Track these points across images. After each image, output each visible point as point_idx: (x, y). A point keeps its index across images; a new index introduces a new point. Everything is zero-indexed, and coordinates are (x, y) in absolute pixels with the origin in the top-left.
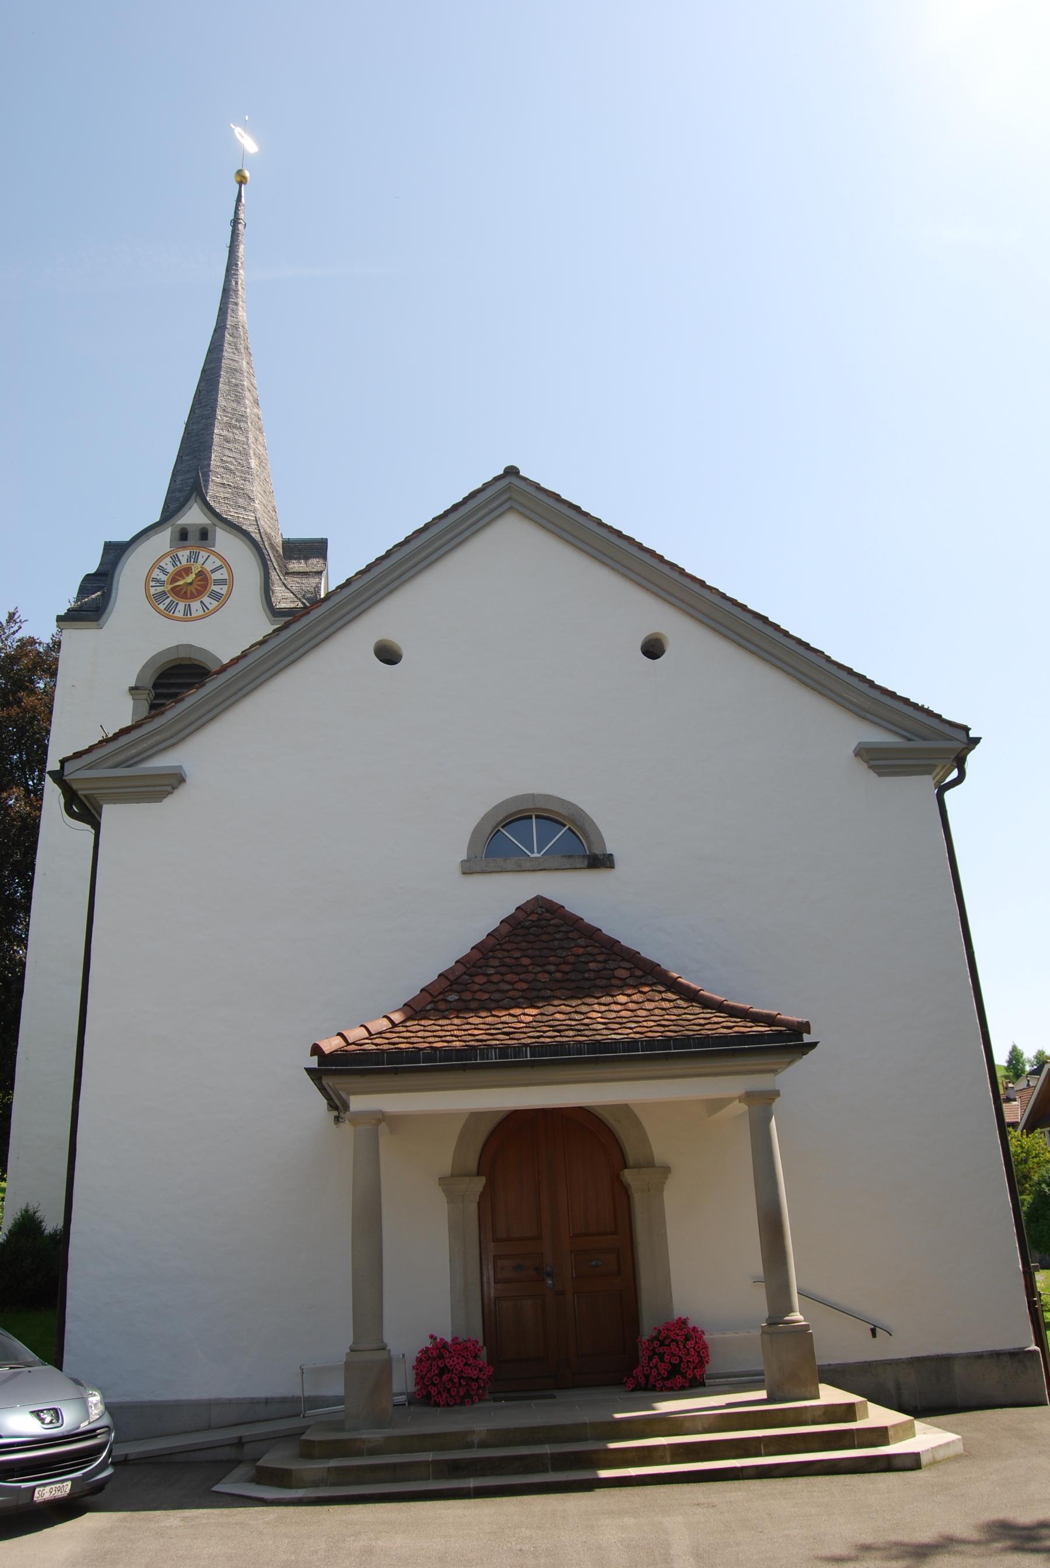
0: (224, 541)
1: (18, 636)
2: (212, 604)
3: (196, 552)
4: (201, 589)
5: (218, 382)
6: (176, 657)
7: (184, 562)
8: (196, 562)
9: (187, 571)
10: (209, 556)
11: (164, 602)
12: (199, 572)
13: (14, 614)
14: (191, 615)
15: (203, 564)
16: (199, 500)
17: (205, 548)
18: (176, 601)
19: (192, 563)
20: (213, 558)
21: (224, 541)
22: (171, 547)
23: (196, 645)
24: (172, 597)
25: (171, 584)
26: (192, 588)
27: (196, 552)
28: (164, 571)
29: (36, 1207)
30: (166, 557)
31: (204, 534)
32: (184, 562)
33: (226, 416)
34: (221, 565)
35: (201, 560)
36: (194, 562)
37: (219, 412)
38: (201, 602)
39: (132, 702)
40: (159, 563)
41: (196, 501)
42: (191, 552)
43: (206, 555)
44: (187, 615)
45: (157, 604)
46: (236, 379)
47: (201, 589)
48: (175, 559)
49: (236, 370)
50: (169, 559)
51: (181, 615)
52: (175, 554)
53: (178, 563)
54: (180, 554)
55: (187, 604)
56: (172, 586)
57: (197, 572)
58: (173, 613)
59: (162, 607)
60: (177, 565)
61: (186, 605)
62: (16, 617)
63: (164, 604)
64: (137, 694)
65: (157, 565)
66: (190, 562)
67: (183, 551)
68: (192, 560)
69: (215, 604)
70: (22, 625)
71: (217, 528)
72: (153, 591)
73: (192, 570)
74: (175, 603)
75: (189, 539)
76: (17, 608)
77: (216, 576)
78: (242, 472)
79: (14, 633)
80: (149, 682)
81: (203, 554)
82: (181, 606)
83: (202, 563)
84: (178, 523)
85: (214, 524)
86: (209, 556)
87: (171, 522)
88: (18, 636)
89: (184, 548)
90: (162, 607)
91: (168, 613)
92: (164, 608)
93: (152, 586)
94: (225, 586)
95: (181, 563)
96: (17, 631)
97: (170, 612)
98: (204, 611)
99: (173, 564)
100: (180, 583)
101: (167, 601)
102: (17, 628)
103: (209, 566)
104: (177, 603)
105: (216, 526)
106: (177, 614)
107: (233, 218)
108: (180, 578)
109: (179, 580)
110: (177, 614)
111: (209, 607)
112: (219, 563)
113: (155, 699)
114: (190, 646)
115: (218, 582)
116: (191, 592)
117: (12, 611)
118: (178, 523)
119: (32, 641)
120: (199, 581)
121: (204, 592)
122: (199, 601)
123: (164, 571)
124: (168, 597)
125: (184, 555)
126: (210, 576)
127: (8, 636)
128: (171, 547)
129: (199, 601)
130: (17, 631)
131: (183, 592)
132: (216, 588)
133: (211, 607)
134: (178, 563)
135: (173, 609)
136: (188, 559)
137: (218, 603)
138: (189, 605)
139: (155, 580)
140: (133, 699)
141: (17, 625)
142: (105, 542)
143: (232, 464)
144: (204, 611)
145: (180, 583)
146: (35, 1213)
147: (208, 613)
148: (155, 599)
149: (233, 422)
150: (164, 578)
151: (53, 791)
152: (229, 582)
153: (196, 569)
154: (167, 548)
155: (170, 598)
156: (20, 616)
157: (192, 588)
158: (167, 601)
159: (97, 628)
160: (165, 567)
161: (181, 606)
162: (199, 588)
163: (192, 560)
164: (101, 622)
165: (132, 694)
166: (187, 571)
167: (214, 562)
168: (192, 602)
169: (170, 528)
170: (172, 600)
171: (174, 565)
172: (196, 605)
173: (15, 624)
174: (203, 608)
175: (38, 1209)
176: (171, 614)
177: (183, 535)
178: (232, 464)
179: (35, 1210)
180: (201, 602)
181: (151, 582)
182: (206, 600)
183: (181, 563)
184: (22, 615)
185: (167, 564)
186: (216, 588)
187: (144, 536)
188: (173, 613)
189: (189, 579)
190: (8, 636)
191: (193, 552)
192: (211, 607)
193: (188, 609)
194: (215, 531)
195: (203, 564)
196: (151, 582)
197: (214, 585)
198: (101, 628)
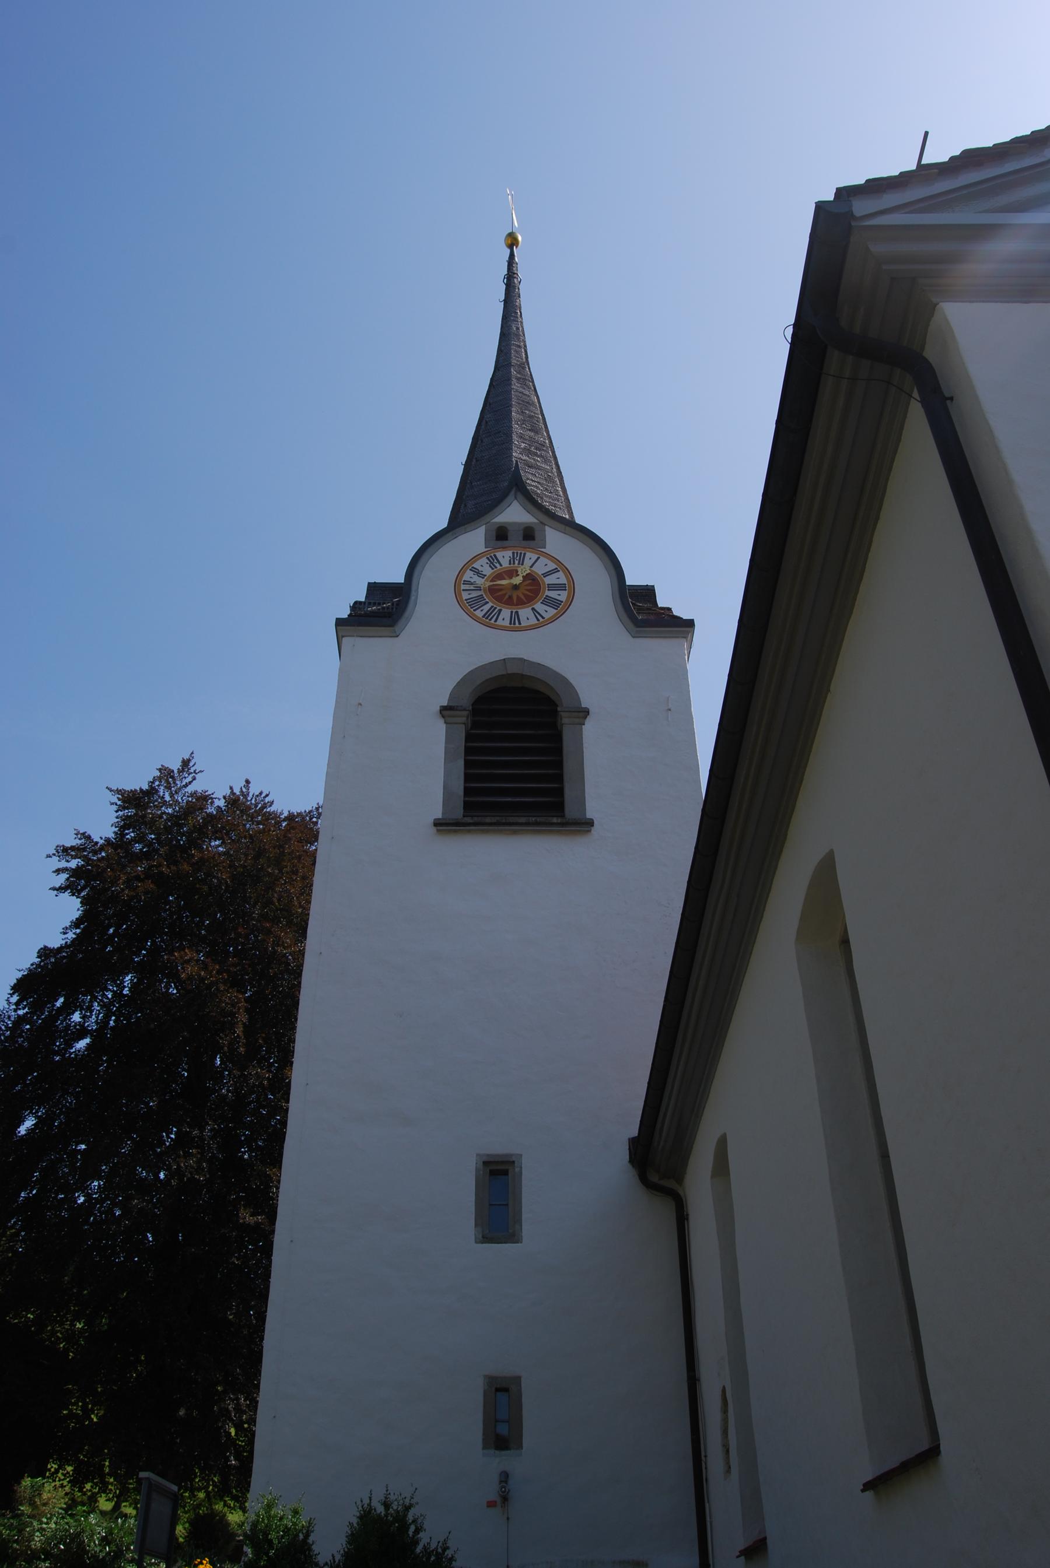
0: (554, 540)
1: (190, 789)
2: (550, 612)
3: (521, 553)
4: (532, 595)
5: (511, 412)
6: (504, 673)
7: (505, 563)
8: (522, 564)
9: (512, 573)
10: (538, 558)
11: (481, 609)
12: (527, 574)
13: (189, 760)
14: (520, 623)
15: (531, 567)
16: (520, 496)
17: (533, 549)
18: (498, 608)
19: (516, 565)
20: (543, 560)
21: (554, 540)
22: (486, 548)
23: (531, 660)
24: (493, 602)
25: (491, 581)
26: (519, 593)
27: (521, 553)
28: (478, 573)
29: (408, 1496)
30: (481, 558)
31: (529, 535)
32: (505, 563)
33: (524, 443)
34: (544, 577)
35: (528, 562)
36: (519, 564)
37: (514, 437)
38: (533, 609)
39: (444, 726)
40: (472, 564)
41: (516, 498)
42: (513, 553)
43: (534, 557)
44: (514, 624)
45: (472, 610)
46: (529, 411)
47: (532, 595)
48: (493, 561)
49: (528, 403)
50: (484, 560)
51: (507, 623)
52: (492, 555)
53: (497, 565)
54: (499, 555)
55: (514, 611)
56: (492, 583)
57: (525, 574)
58: (496, 621)
59: (479, 614)
60: (496, 567)
61: (512, 612)
62: (191, 764)
63: (482, 610)
64: (450, 716)
65: (469, 565)
66: (514, 563)
67: (505, 552)
68: (517, 562)
69: (552, 612)
70: (196, 776)
71: (547, 528)
72: (465, 596)
73: (517, 572)
74: (496, 610)
75: (509, 539)
76: (192, 753)
77: (550, 580)
78: (550, 497)
79: (186, 785)
80: (466, 701)
81: (530, 557)
82: (506, 613)
83: (530, 565)
84: (493, 521)
85: (541, 523)
86: (538, 558)
87: (487, 518)
88: (190, 789)
89: (504, 548)
90: (479, 614)
91: (489, 620)
92: (483, 615)
93: (463, 590)
94: (564, 591)
95: (501, 565)
96: (190, 783)
97: (490, 620)
98: (538, 620)
99: (490, 566)
100: (504, 582)
101: (486, 608)
102: (191, 780)
103: (540, 569)
104: (500, 611)
105: (545, 525)
106: (500, 622)
107: (506, 273)
108: (506, 577)
109: (505, 579)
110: (500, 622)
111: (544, 616)
112: (552, 566)
113: (472, 728)
114: (522, 660)
115: (552, 587)
116: (518, 597)
117: (186, 757)
118: (493, 521)
119: (204, 799)
120: (527, 585)
121: (525, 604)
122: (531, 608)
123: (478, 573)
124: (487, 603)
125: (504, 557)
126: (543, 580)
127: (180, 789)
128: (486, 548)
129: (531, 608)
130: (190, 783)
131: (507, 597)
132: (553, 594)
133: (547, 616)
134: (497, 565)
135: (495, 617)
136: (510, 561)
137: (556, 611)
138: (517, 613)
139: (466, 582)
140: (445, 722)
141: (191, 776)
142: (369, 583)
143: (537, 487)
144: (538, 620)
145: (504, 582)
146: (407, 1508)
147: (542, 623)
148: (469, 606)
149: (532, 449)
150: (479, 581)
151: (333, 838)
152: (569, 587)
153: (524, 570)
154: (482, 548)
155: (490, 604)
156: (195, 763)
157: (519, 593)
158: (486, 608)
159: (391, 637)
160: (480, 569)
161: (506, 613)
162: (523, 597)
163: (517, 562)
164: (397, 628)
165: (443, 717)
166: (512, 573)
167: (546, 565)
168: (520, 609)
169: (484, 526)
170: (492, 607)
171: (492, 565)
172: (525, 613)
173: (189, 774)
174: (535, 614)
175: (413, 1501)
176: (492, 621)
177: (501, 535)
178: (537, 487)
179: (407, 1502)
180: (533, 609)
181: (462, 585)
182: (539, 607)
183: (501, 565)
184: (198, 764)
185: (483, 565)
186: (553, 594)
187: (450, 533)
188: (496, 621)
189: (517, 580)
190: (180, 789)
191: (517, 553)
192: (547, 616)
193: (515, 618)
194: (545, 531)
195: (531, 567)
196: (462, 585)
197: (548, 590)
198: (397, 636)
